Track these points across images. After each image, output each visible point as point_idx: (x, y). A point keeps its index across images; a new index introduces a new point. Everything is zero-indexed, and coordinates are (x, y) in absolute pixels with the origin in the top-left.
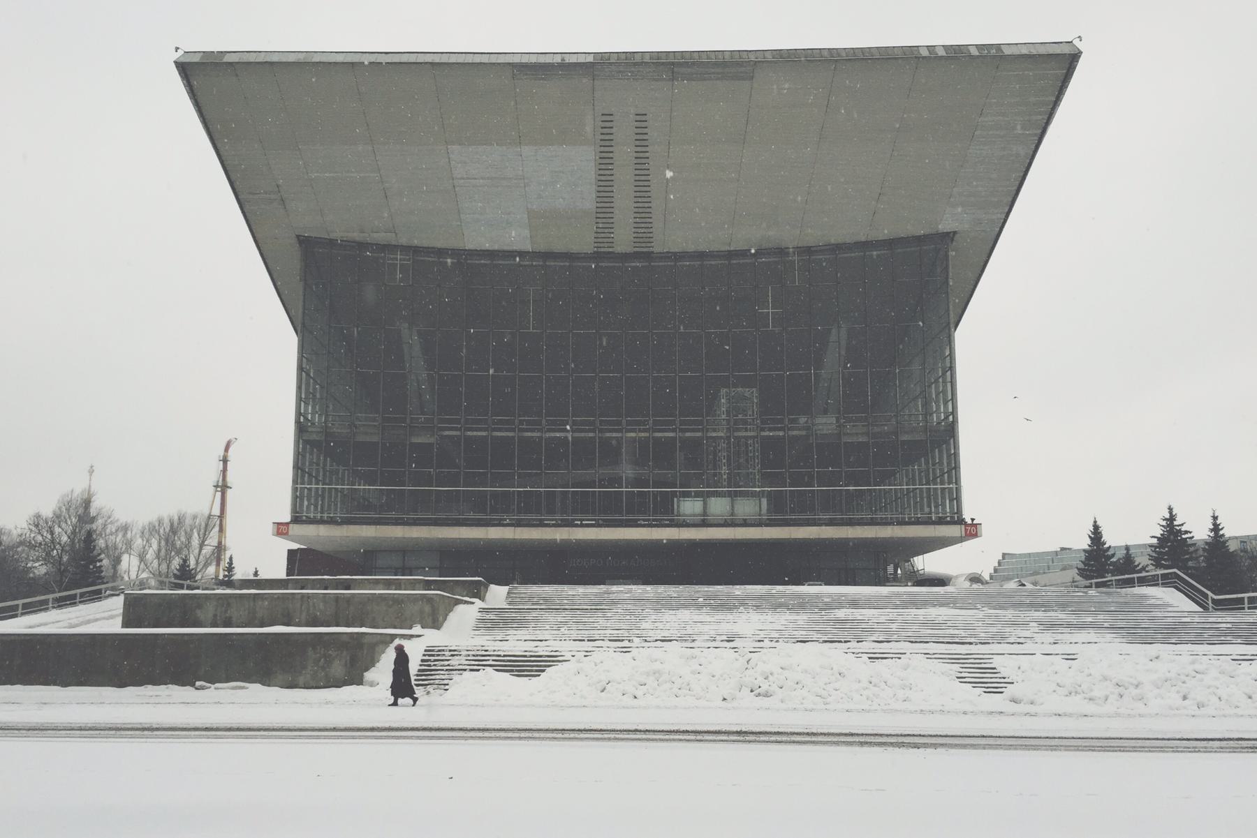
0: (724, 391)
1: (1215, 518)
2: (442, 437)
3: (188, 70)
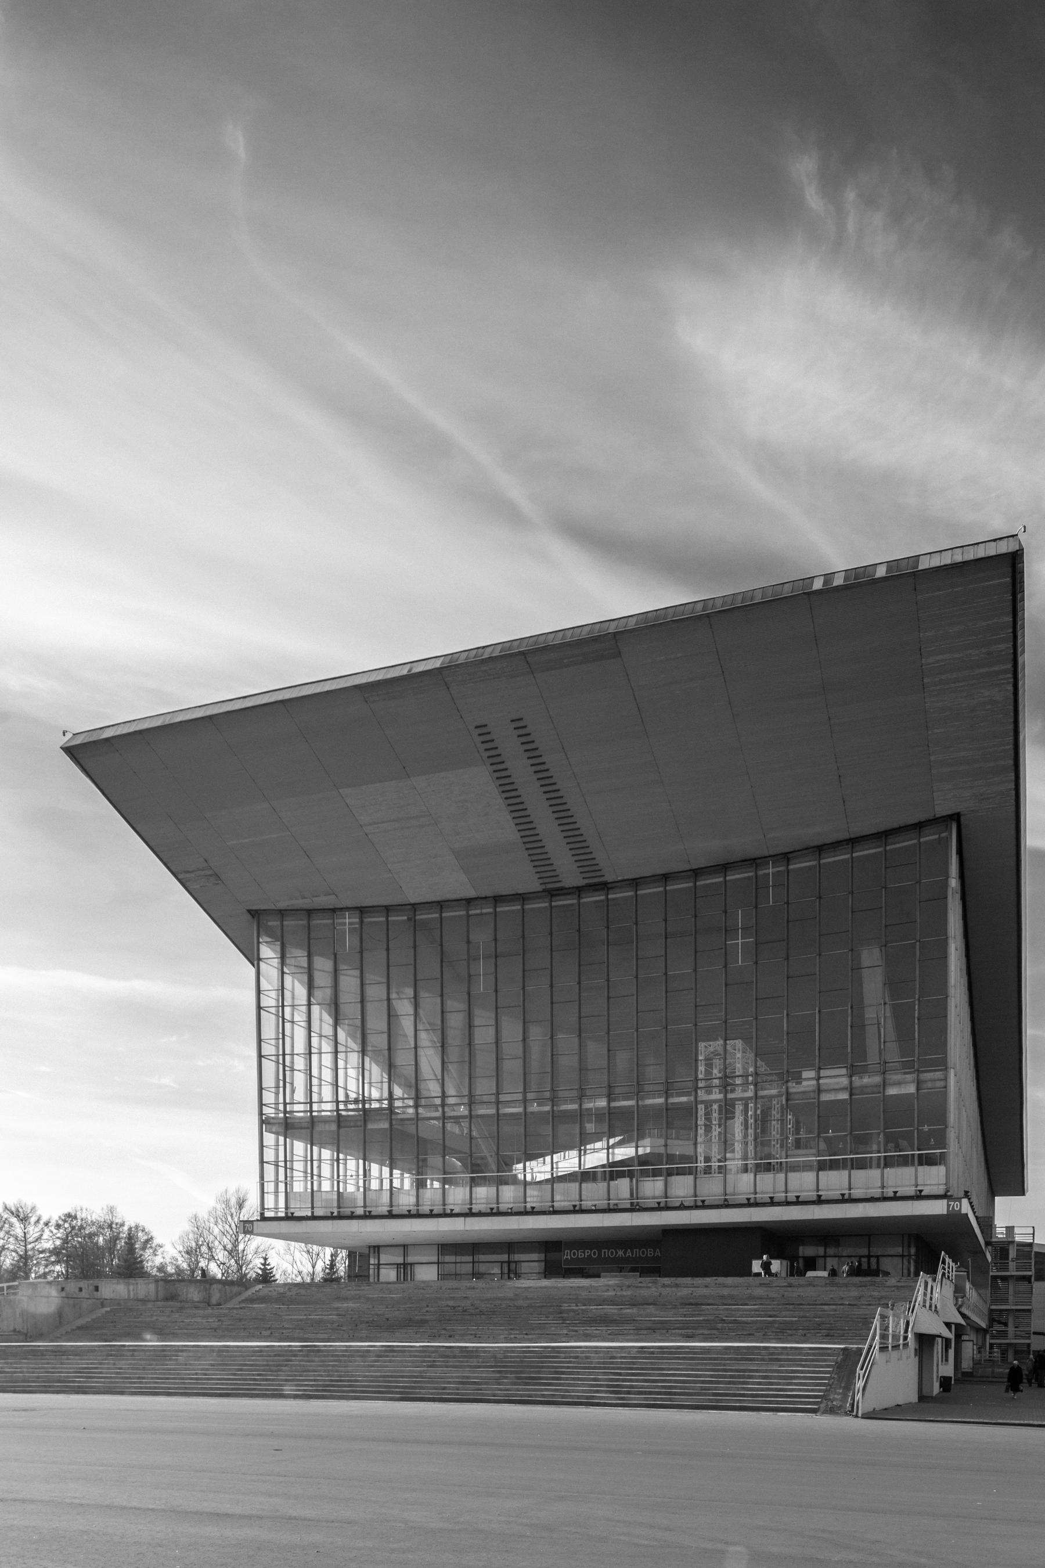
3: (70, 751)
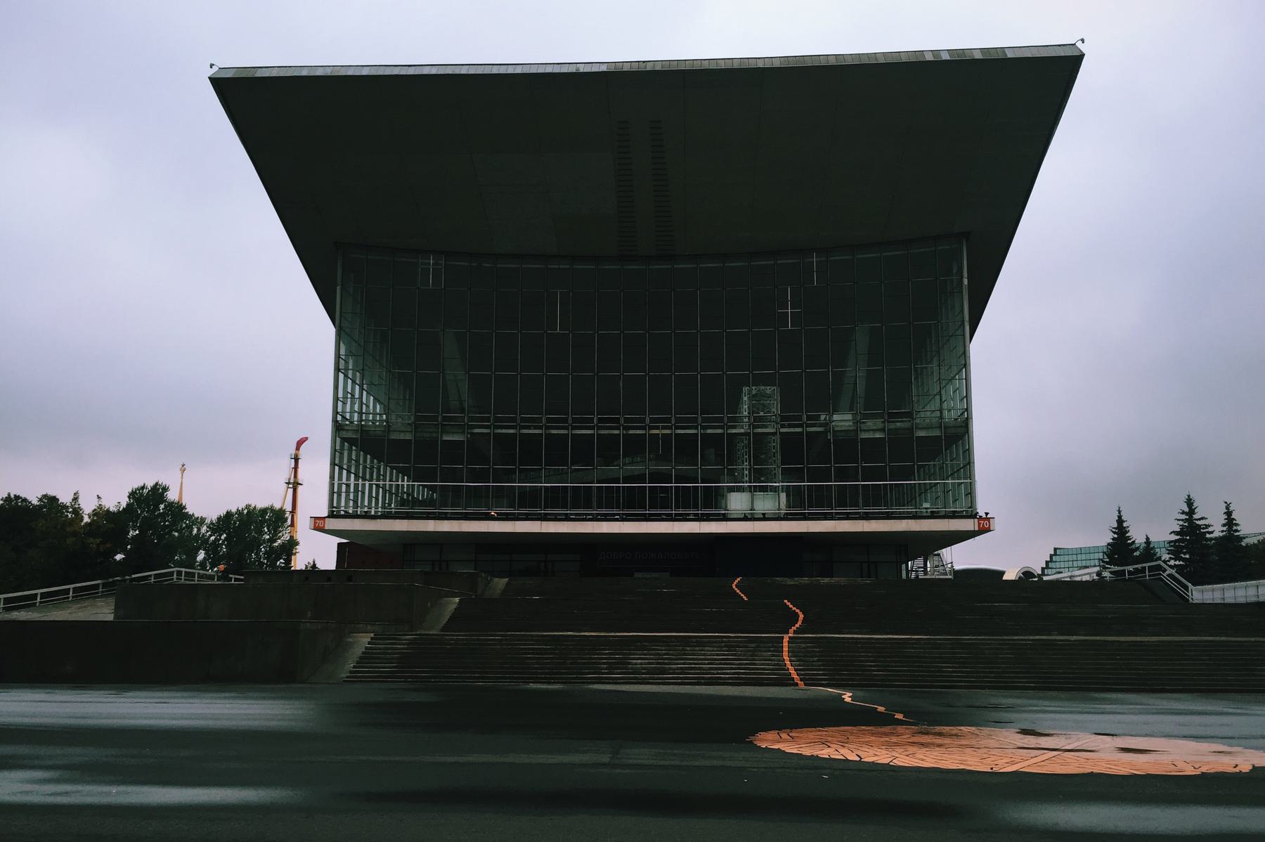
0: (745, 389)
1: (1229, 513)
2: (473, 434)
3: (216, 82)
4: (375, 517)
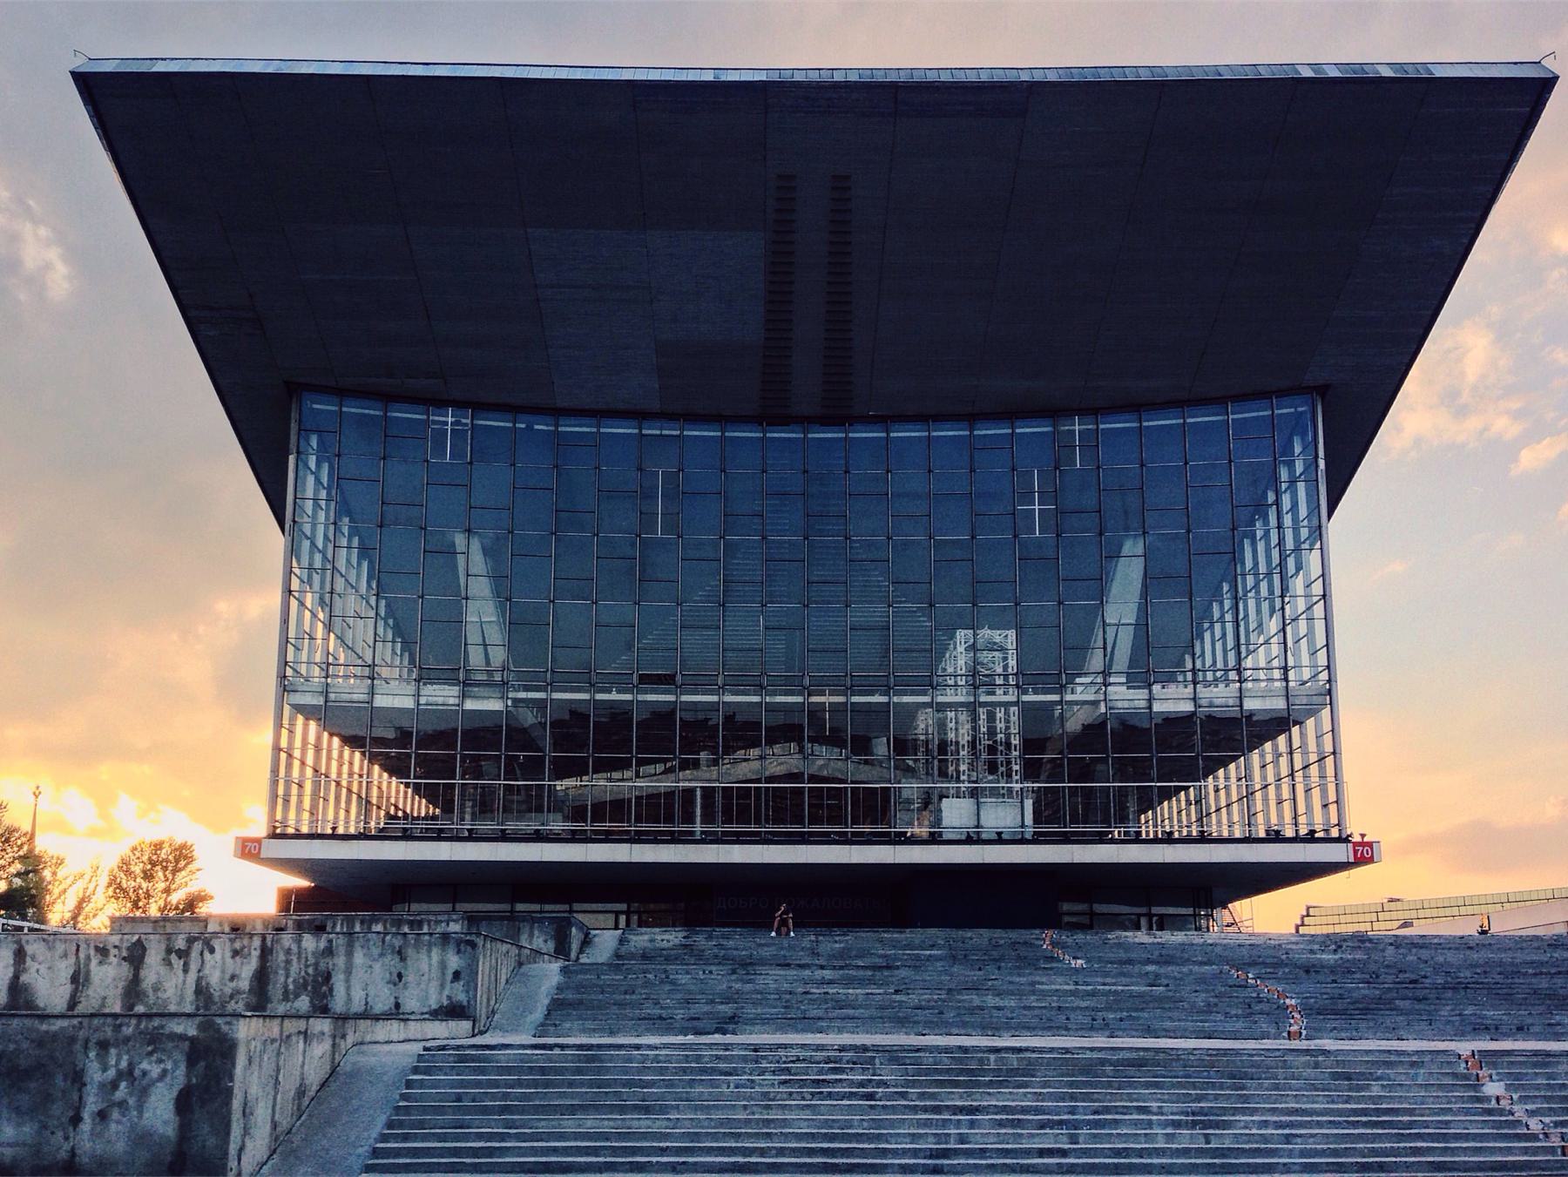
4: (347, 837)
